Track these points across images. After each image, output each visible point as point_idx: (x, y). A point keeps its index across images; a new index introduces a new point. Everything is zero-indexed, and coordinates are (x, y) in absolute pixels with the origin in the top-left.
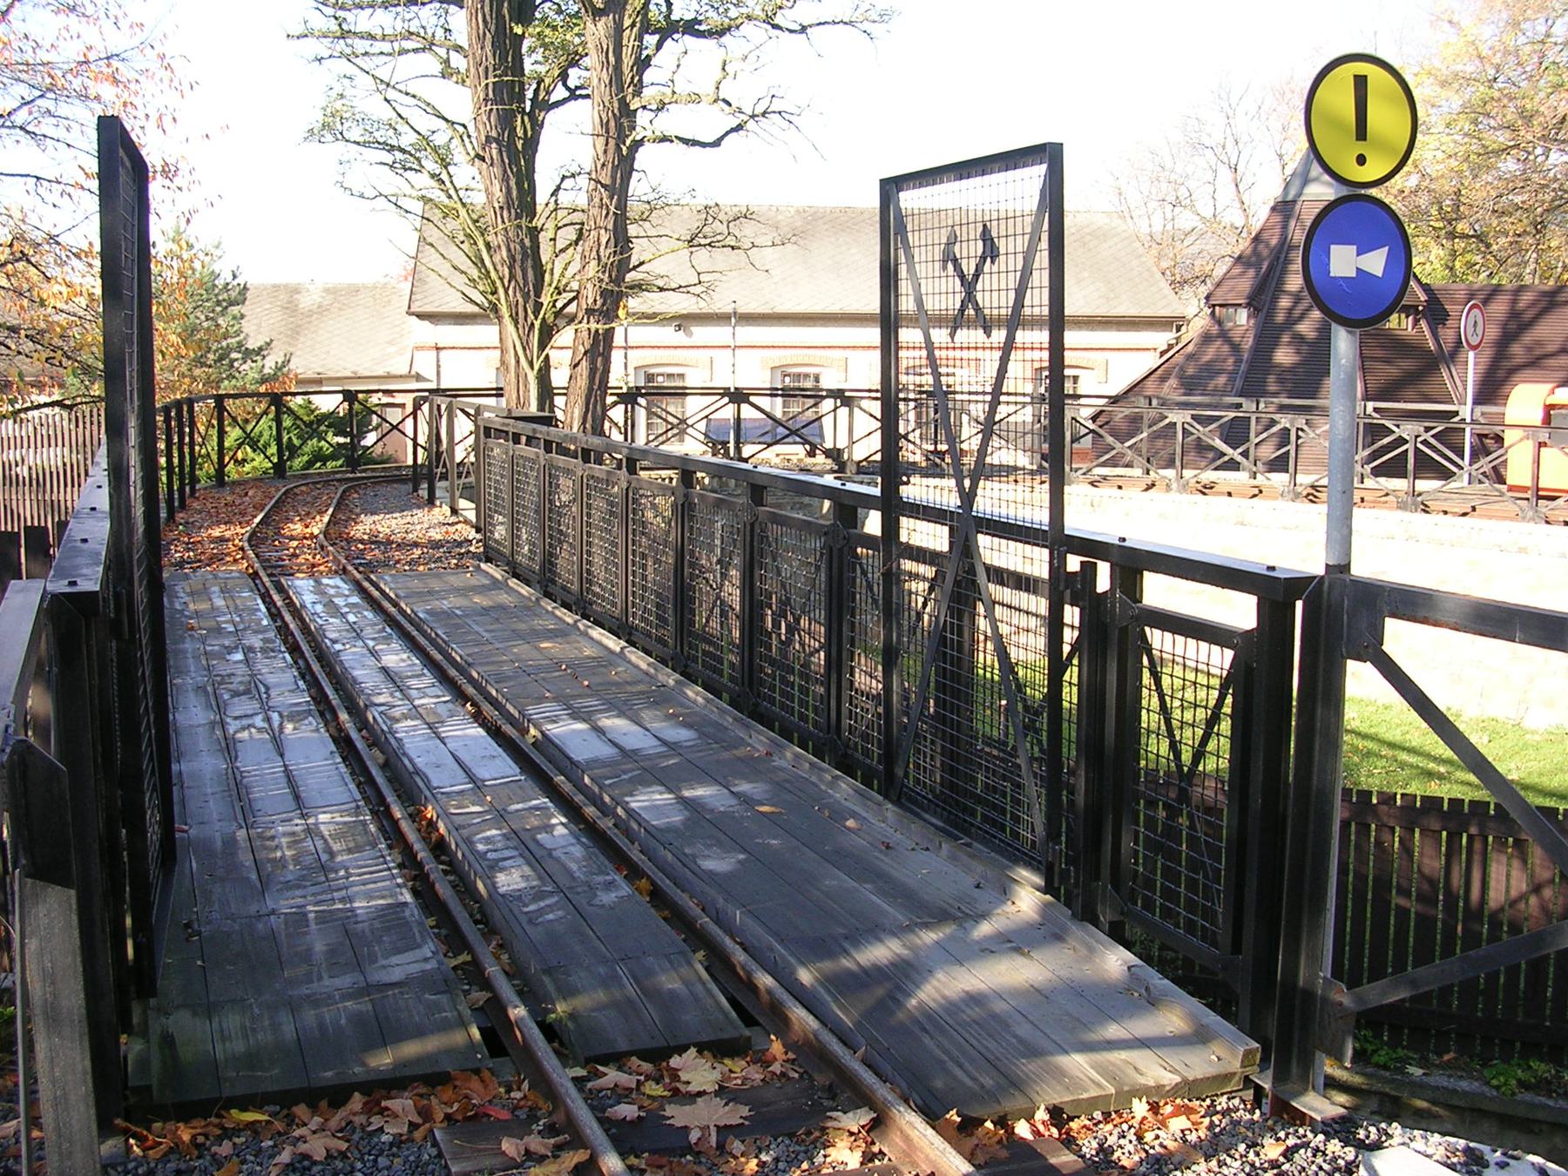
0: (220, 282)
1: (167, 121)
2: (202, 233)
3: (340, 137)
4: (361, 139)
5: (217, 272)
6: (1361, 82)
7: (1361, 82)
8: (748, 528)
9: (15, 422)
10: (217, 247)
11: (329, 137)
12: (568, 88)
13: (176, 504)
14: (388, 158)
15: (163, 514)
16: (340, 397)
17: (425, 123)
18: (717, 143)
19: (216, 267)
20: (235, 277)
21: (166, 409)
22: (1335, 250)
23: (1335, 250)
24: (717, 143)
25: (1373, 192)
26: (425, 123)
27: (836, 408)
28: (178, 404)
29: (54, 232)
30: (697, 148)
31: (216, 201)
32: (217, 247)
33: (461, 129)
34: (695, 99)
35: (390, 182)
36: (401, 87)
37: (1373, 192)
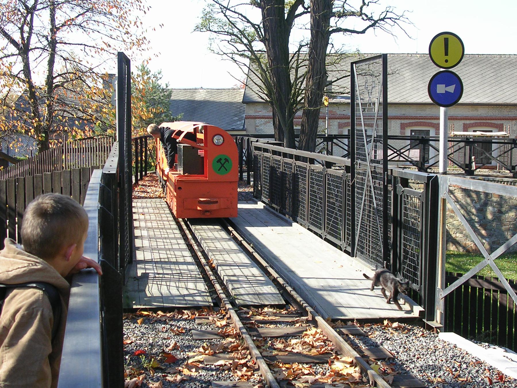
0: (161, 87)
1: (138, 24)
2: (153, 68)
3: (209, 29)
4: (216, 30)
5: (160, 84)
6: (446, 41)
7: (446, 41)
8: (345, 181)
9: (237, 299)
10: (159, 74)
11: (204, 29)
12: (305, 8)
13: (139, 178)
14: (229, 38)
15: (134, 181)
16: (475, 173)
17: (241, 25)
18: (363, 32)
19: (159, 82)
20: (167, 87)
21: (136, 139)
22: (439, 86)
23: (439, 86)
24: (363, 32)
25: (450, 70)
26: (241, 25)
27: (512, 149)
28: (141, 138)
29: (123, 43)
30: (355, 34)
31: (159, 55)
32: (159, 74)
33: (257, 27)
34: (353, 14)
35: (229, 49)
36: (233, 9)
37: (450, 70)
